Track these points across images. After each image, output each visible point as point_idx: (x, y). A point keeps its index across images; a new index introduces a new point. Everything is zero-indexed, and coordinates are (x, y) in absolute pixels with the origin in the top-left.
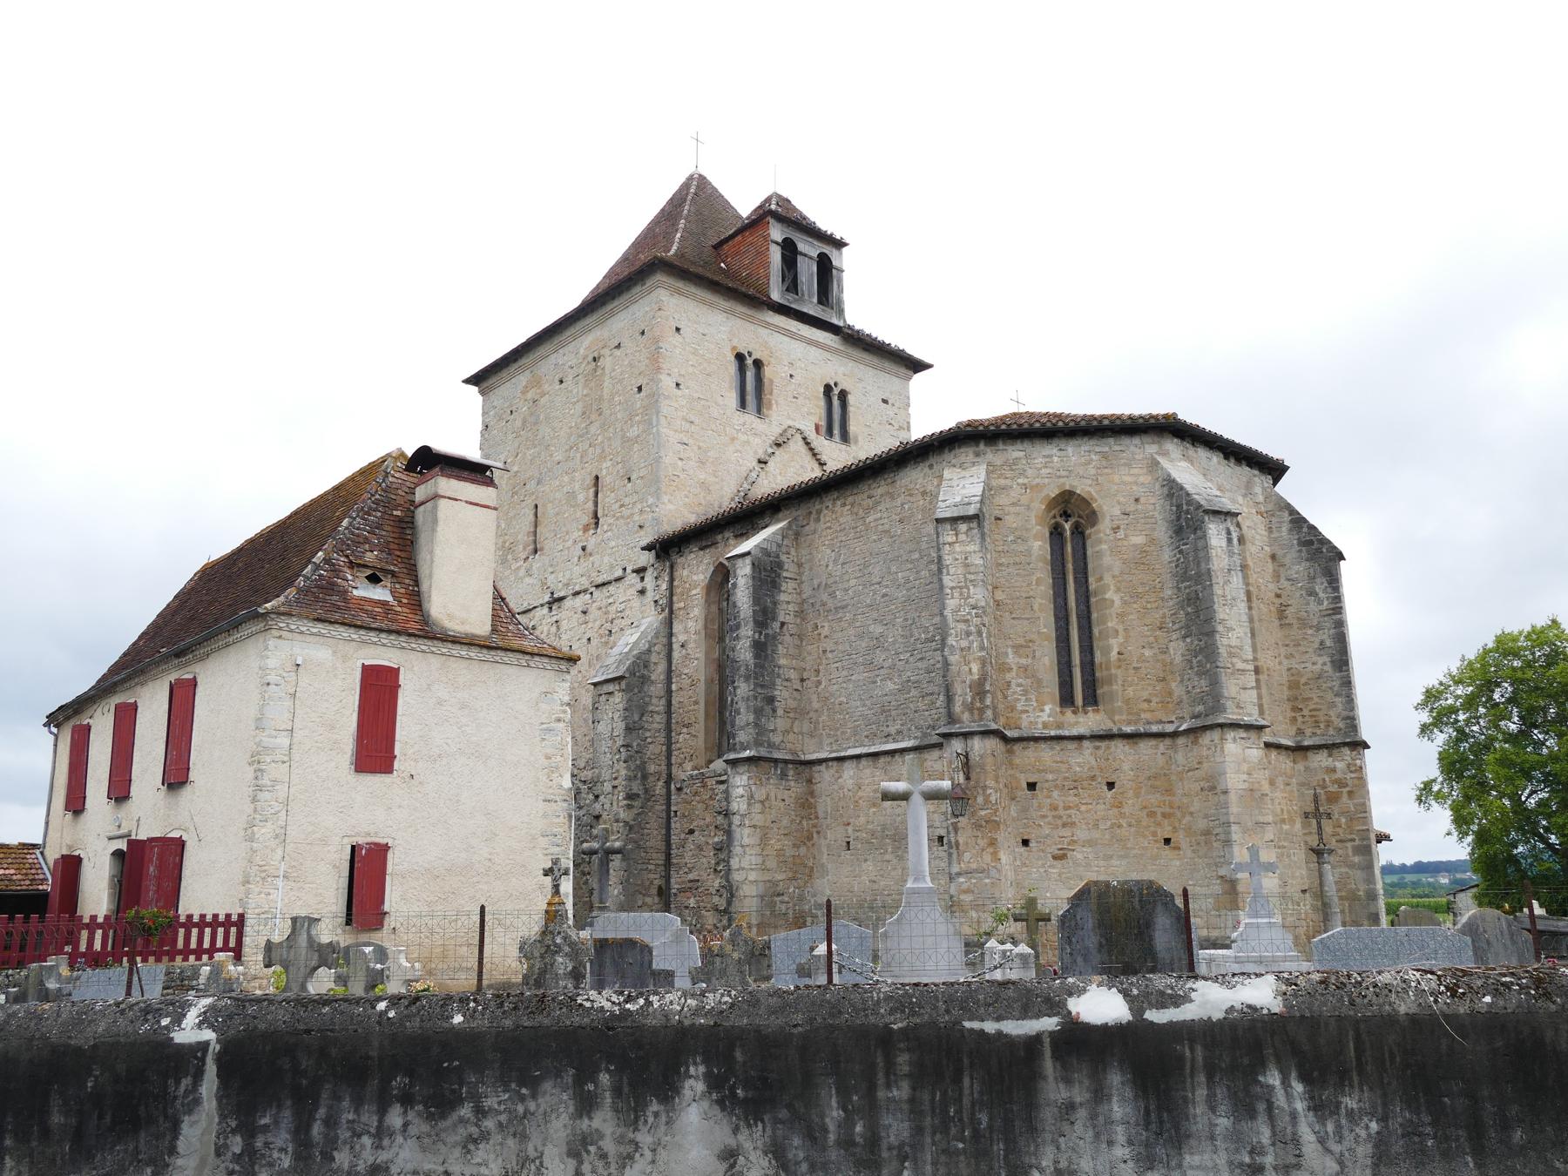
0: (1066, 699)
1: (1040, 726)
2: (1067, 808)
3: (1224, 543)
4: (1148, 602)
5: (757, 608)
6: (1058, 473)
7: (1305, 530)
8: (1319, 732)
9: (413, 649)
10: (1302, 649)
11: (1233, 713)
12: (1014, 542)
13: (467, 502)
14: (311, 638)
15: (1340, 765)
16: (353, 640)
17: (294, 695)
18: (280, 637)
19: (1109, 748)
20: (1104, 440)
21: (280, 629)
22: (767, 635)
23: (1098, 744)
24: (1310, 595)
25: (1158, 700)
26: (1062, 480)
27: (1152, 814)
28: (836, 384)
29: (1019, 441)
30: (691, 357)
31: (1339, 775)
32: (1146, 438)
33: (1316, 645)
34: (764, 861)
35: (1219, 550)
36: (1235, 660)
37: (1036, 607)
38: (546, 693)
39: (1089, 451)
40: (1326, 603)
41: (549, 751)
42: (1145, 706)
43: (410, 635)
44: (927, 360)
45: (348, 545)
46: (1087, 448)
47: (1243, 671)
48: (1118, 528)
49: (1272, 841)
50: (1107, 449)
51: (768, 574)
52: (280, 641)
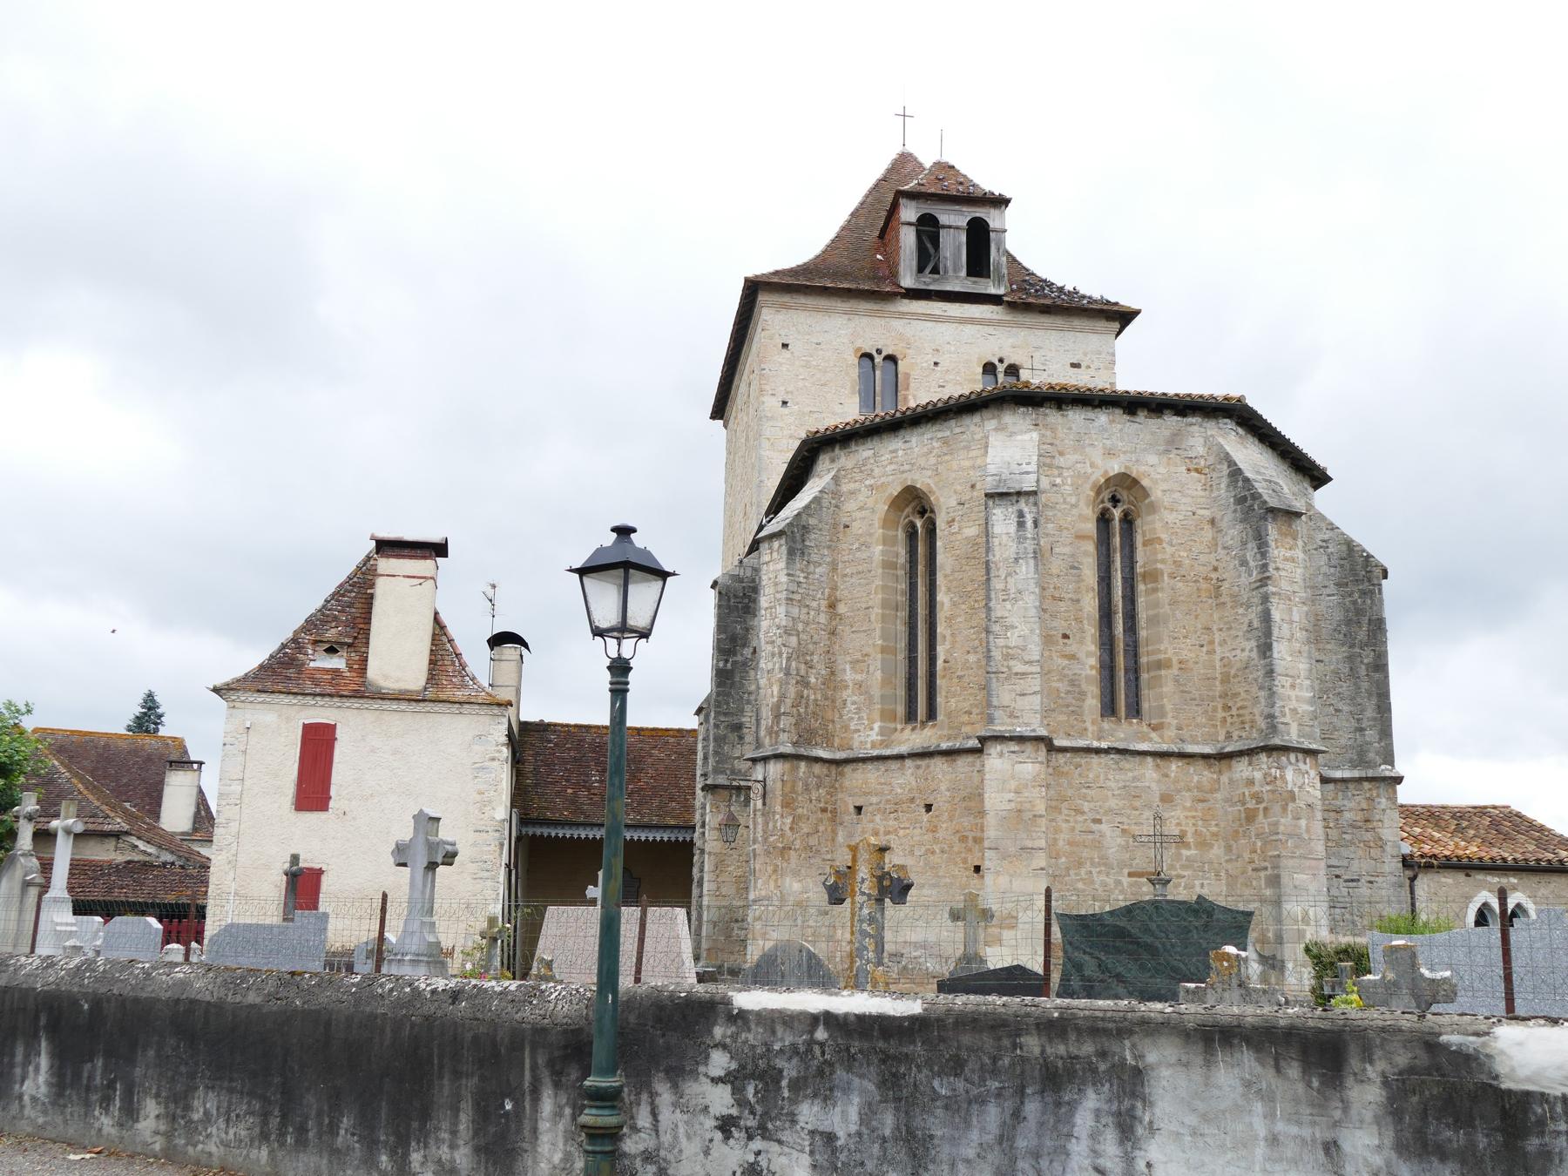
0: (1109, 708)
1: (869, 746)
2: (888, 833)
3: (1013, 528)
4: (976, 601)
5: (723, 636)
6: (902, 468)
7: (1240, 484)
8: (1244, 735)
9: (348, 707)
10: (1233, 632)
11: (1002, 724)
12: (858, 549)
13: (404, 576)
14: (258, 706)
15: (1258, 775)
16: (295, 704)
17: (245, 752)
18: (234, 707)
19: (928, 767)
20: (946, 424)
21: (233, 701)
22: (735, 663)
23: (919, 762)
24: (1241, 565)
25: (978, 711)
26: (904, 475)
27: (963, 839)
28: (1001, 361)
29: (869, 439)
30: (801, 370)
31: (1257, 788)
32: (986, 414)
33: (1245, 627)
34: (718, 888)
35: (1005, 538)
36: (1012, 663)
37: (873, 618)
38: (480, 736)
39: (931, 439)
40: (1255, 573)
41: (482, 787)
42: (965, 718)
43: (342, 696)
44: (1135, 306)
45: (316, 625)
46: (929, 436)
47: (1024, 674)
48: (953, 520)
49: (1042, 869)
50: (948, 433)
51: (738, 600)
52: (235, 710)
